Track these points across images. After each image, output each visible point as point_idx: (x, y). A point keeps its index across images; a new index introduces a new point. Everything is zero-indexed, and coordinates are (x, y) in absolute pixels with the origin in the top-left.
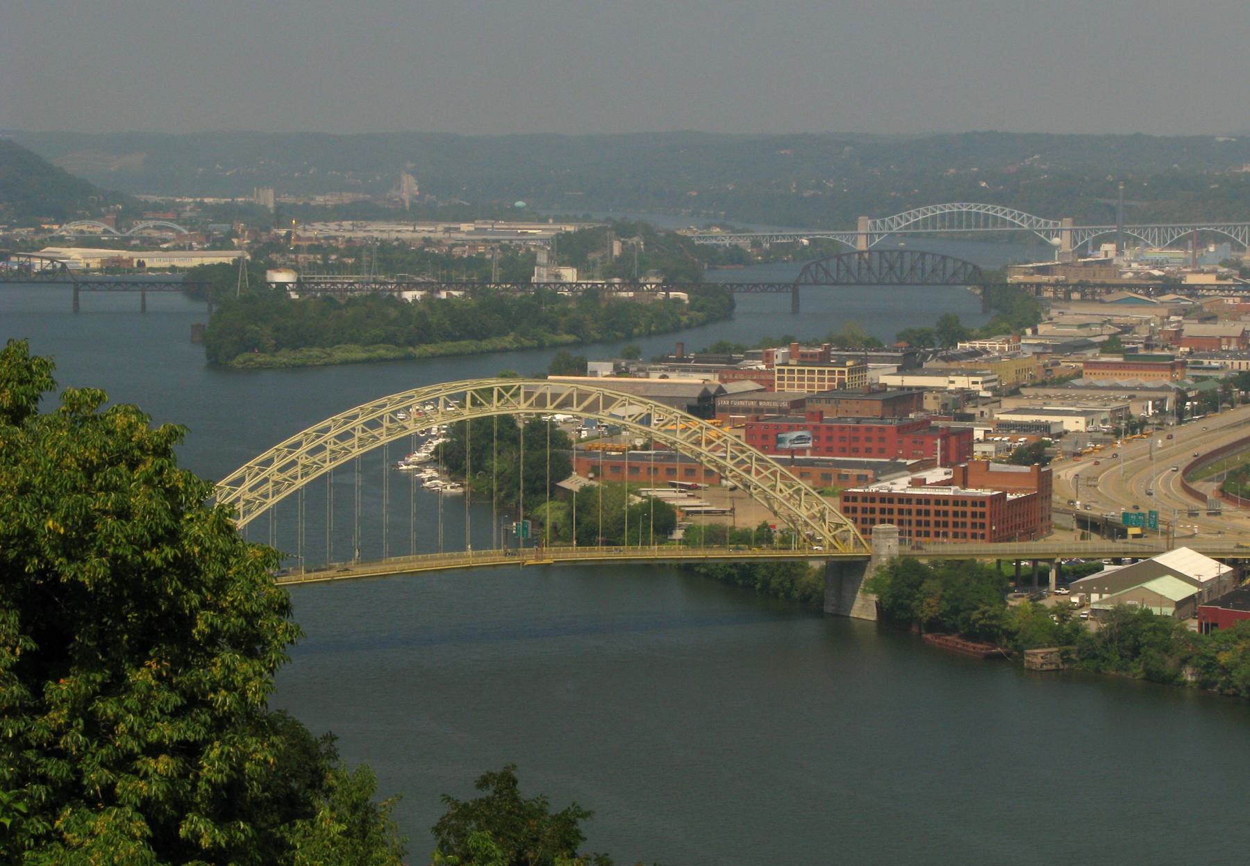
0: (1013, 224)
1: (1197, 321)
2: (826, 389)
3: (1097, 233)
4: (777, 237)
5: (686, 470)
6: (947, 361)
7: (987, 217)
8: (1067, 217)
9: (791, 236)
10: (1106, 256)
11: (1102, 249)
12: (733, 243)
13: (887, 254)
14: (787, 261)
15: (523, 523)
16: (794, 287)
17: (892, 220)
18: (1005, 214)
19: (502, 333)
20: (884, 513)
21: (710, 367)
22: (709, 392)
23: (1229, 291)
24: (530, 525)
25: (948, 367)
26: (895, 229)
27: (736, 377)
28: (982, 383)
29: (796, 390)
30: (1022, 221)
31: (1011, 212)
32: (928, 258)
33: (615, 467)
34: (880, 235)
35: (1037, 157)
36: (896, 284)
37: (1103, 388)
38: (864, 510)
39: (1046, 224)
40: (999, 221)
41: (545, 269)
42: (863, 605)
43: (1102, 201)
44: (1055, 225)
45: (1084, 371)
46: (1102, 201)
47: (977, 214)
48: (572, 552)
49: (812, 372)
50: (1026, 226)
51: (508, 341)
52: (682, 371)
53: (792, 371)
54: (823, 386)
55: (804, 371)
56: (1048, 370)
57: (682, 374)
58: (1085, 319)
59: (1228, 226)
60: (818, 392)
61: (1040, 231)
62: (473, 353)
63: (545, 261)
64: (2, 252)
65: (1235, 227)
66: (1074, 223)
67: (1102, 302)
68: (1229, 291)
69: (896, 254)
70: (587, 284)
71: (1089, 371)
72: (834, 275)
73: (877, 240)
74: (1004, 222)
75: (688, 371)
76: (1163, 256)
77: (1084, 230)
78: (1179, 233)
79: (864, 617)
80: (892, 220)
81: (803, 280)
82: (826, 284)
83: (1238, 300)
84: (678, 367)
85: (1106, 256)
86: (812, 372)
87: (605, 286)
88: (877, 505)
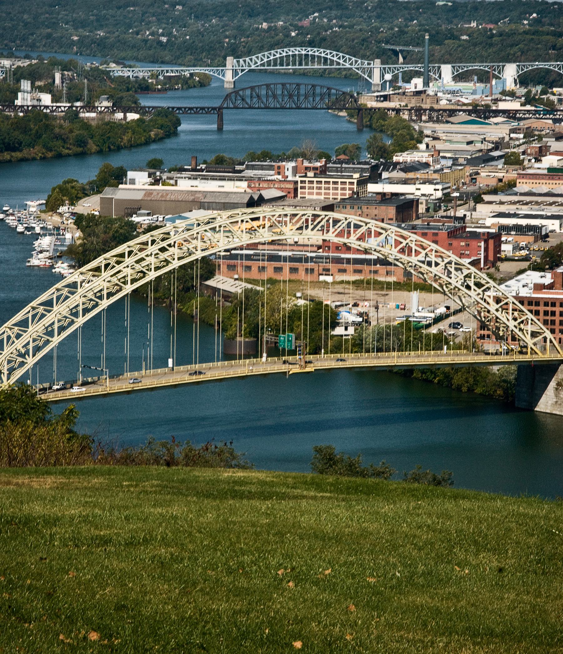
0: (338, 64)
1: (554, 139)
2: (347, 197)
3: (527, 68)
4: (167, 71)
5: (275, 268)
6: (406, 172)
7: (313, 57)
8: (377, 58)
9: (177, 71)
10: (416, 88)
11: (412, 81)
12: (135, 75)
13: (288, 86)
14: (178, 89)
15: (288, 335)
16: (219, 111)
17: (251, 60)
18: (327, 54)
19: (31, 145)
20: (548, 315)
21: (224, 176)
22: (254, 199)
23: (540, 115)
24: (294, 338)
25: (407, 177)
26: (253, 67)
27: (261, 186)
28: (443, 190)
29: (315, 197)
30: (345, 61)
31: (337, 55)
32: (302, 87)
33: (231, 266)
34: (242, 70)
35: (316, 14)
36: (231, 108)
37: (540, 195)
38: (546, 313)
39: (362, 64)
40: (329, 61)
41: (29, 95)
42: (556, 402)
43: (389, 47)
44: (369, 64)
45: (518, 181)
46: (389, 47)
47: (318, 57)
48: (321, 360)
49: (328, 183)
50: (347, 65)
51: (37, 151)
52: (202, 179)
53: (311, 182)
54: (345, 195)
55: (321, 182)
56: (472, 179)
57: (203, 181)
58: (470, 138)
59: (217, 70)
60: (342, 199)
61: (358, 69)
62: (10, 161)
63: (29, 89)
64: (561, 61)
65: (498, 66)
66: (382, 63)
67: (448, 122)
68: (540, 115)
69: (294, 86)
70: (65, 107)
71: (521, 181)
72: (248, 101)
73: (240, 74)
74: (332, 62)
75: (208, 179)
76: (458, 88)
77: (390, 68)
78: (522, 70)
79: (558, 413)
80: (251, 60)
81: (225, 106)
82: (258, 108)
83: (550, 122)
84: (199, 175)
85: (416, 88)
86: (328, 183)
87: (30, 108)
88: (542, 308)
